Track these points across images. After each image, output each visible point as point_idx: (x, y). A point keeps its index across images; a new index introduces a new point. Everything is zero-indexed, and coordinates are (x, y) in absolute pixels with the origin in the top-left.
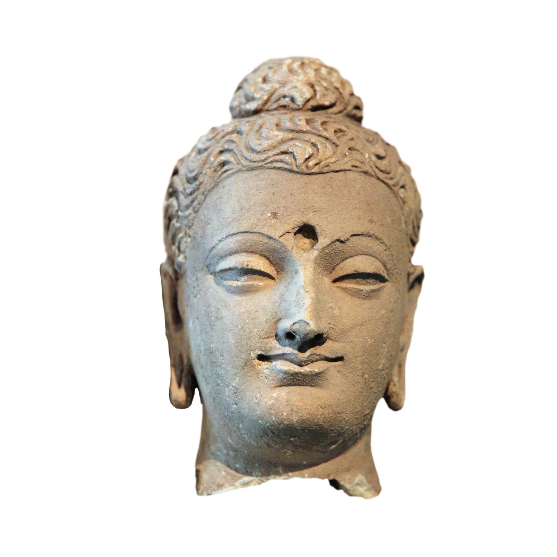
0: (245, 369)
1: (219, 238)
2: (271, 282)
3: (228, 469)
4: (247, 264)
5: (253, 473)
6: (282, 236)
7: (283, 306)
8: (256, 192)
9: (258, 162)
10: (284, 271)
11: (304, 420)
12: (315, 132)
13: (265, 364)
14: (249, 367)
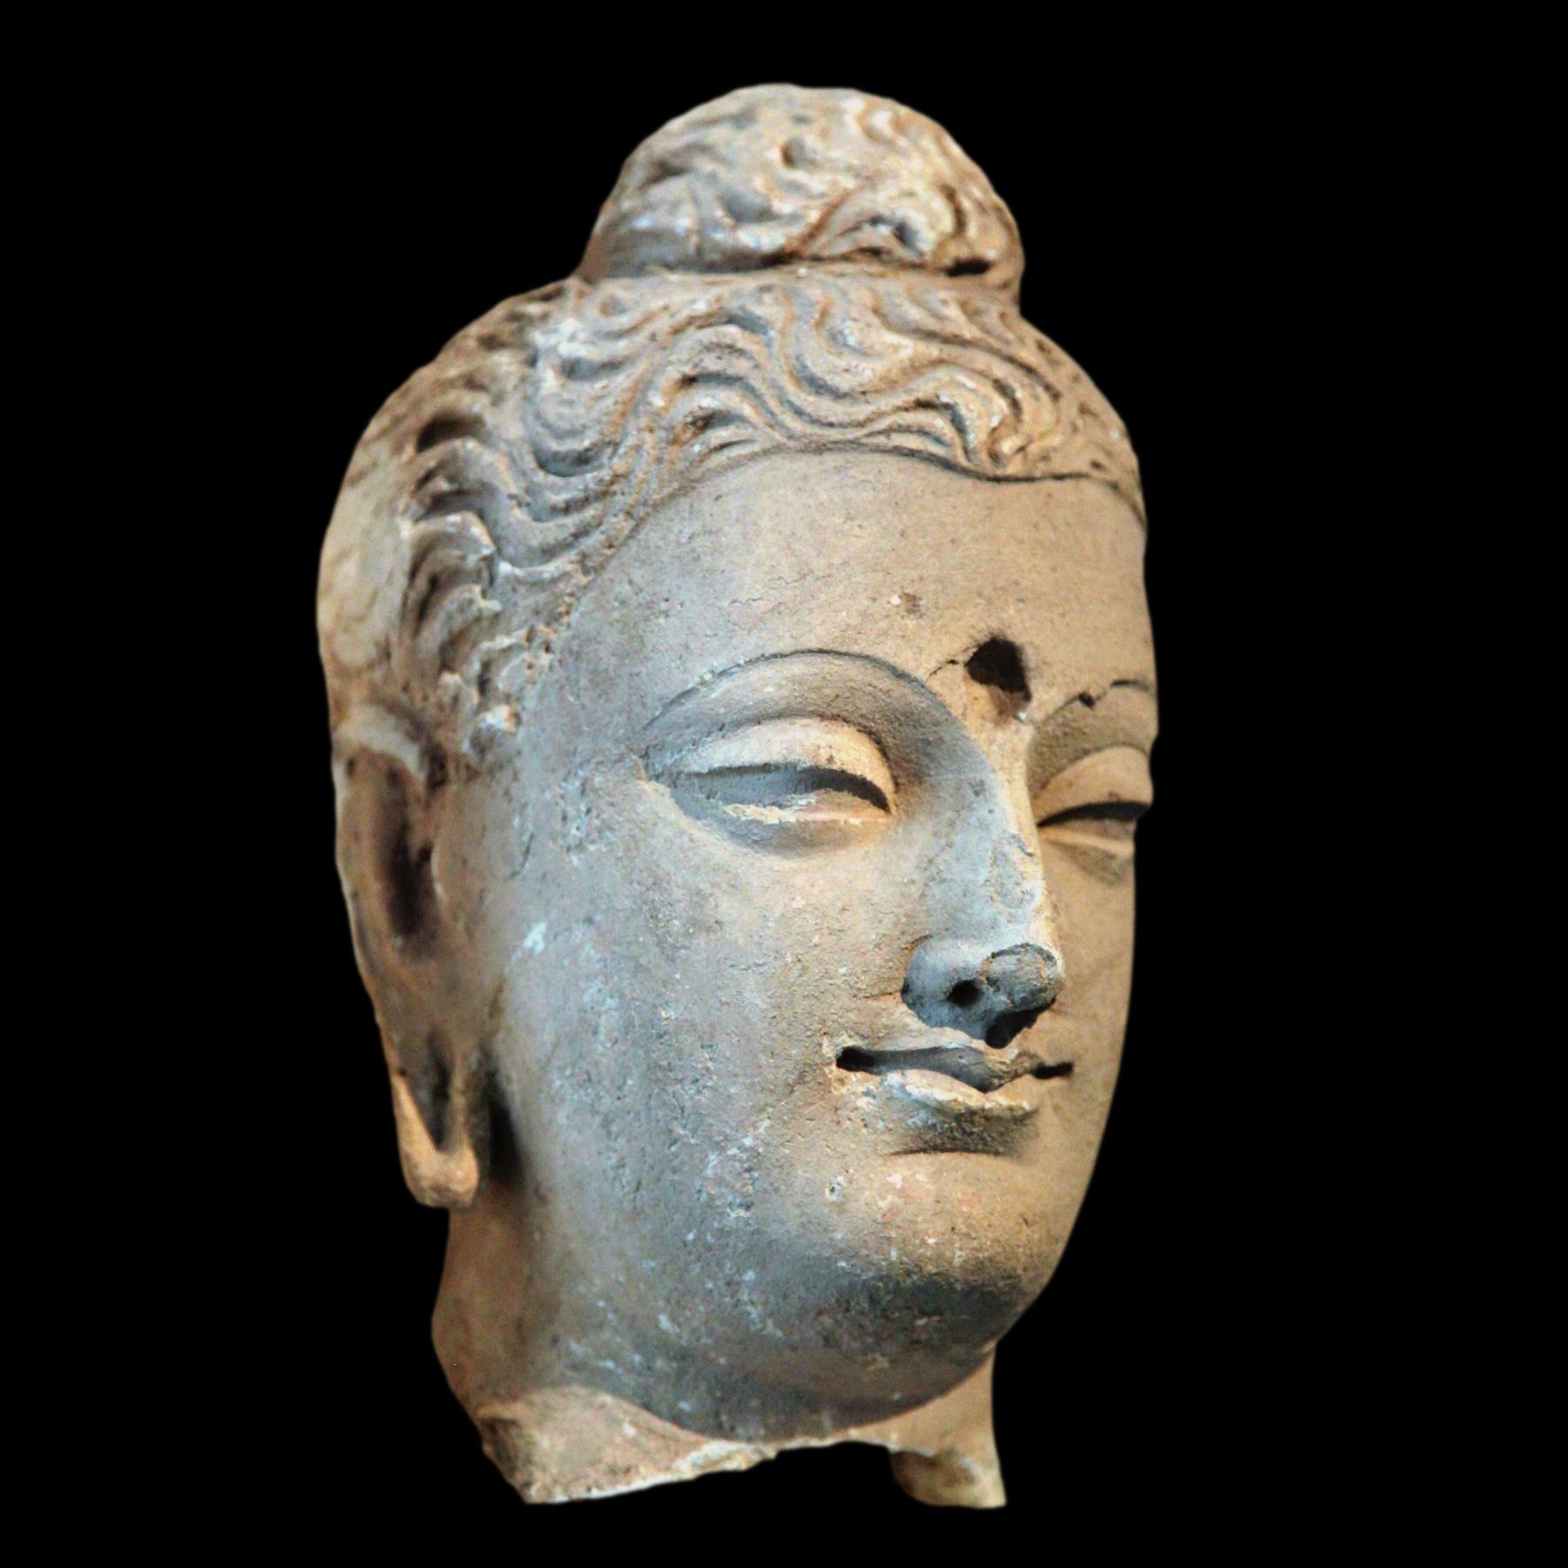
0: (797, 1093)
1: (715, 664)
2: (871, 813)
3: (645, 1416)
4: (827, 756)
5: (740, 1431)
8: (845, 523)
9: (842, 425)
10: (920, 783)
11: (982, 1263)
12: (997, 345)
13: (858, 1081)
14: (811, 1088)
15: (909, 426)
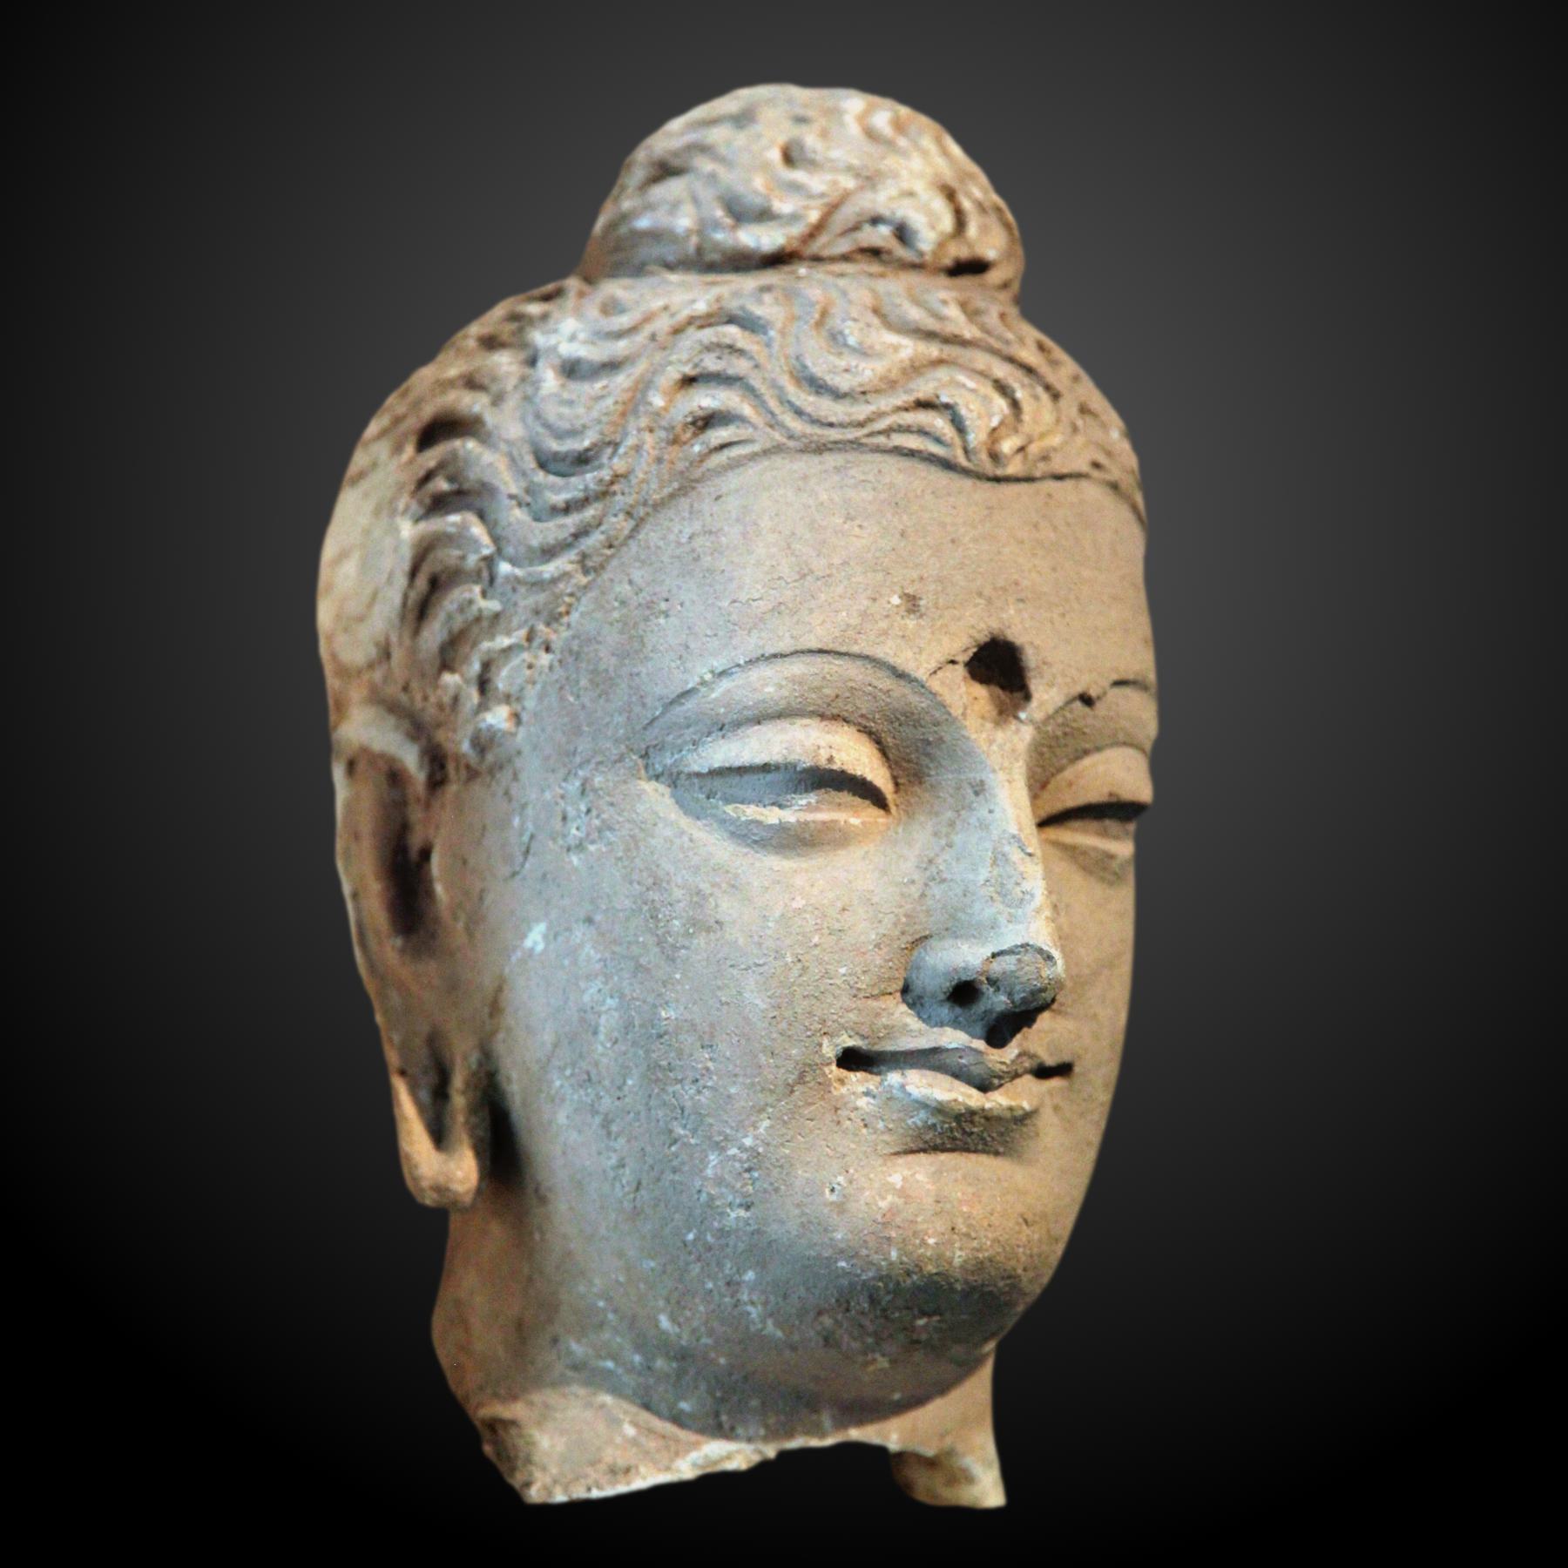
0: (797, 1093)
1: (715, 664)
2: (871, 813)
3: (645, 1416)
4: (827, 756)
5: (740, 1431)
7: (938, 897)
8: (845, 523)
9: (842, 425)
10: (920, 783)
11: (982, 1263)
12: (997, 345)
13: (858, 1081)
14: (811, 1088)
15: (909, 426)
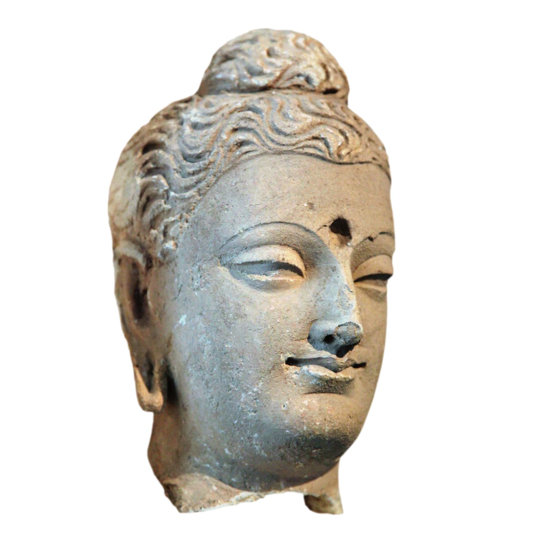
0: (272, 373)
1: (244, 226)
2: (297, 277)
3: (220, 483)
4: (282, 258)
5: (252, 488)
6: (319, 229)
7: (320, 306)
8: (288, 178)
9: (287, 145)
10: (314, 267)
11: (335, 431)
12: (340, 118)
13: (293, 369)
14: (277, 371)
15: (310, 145)
